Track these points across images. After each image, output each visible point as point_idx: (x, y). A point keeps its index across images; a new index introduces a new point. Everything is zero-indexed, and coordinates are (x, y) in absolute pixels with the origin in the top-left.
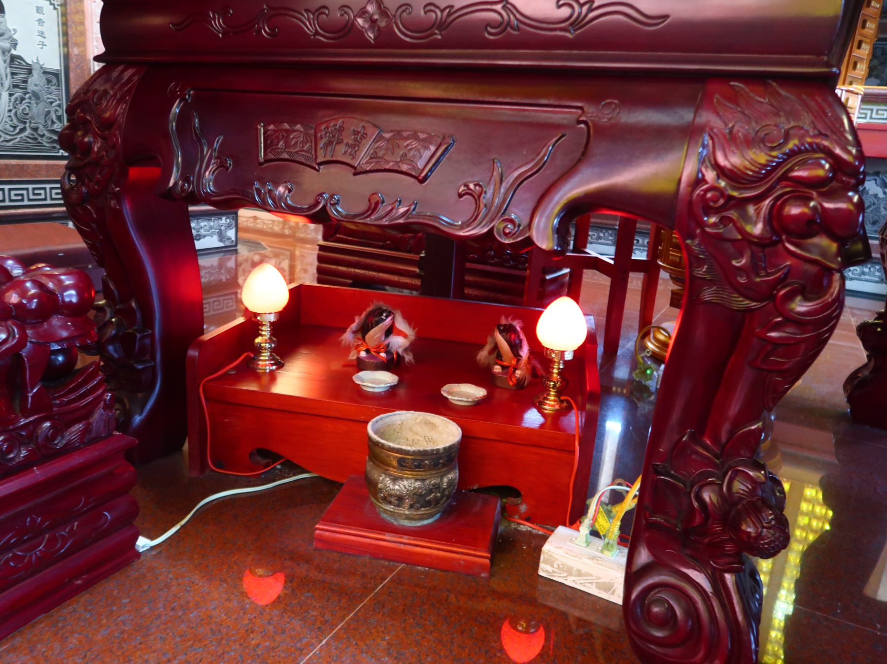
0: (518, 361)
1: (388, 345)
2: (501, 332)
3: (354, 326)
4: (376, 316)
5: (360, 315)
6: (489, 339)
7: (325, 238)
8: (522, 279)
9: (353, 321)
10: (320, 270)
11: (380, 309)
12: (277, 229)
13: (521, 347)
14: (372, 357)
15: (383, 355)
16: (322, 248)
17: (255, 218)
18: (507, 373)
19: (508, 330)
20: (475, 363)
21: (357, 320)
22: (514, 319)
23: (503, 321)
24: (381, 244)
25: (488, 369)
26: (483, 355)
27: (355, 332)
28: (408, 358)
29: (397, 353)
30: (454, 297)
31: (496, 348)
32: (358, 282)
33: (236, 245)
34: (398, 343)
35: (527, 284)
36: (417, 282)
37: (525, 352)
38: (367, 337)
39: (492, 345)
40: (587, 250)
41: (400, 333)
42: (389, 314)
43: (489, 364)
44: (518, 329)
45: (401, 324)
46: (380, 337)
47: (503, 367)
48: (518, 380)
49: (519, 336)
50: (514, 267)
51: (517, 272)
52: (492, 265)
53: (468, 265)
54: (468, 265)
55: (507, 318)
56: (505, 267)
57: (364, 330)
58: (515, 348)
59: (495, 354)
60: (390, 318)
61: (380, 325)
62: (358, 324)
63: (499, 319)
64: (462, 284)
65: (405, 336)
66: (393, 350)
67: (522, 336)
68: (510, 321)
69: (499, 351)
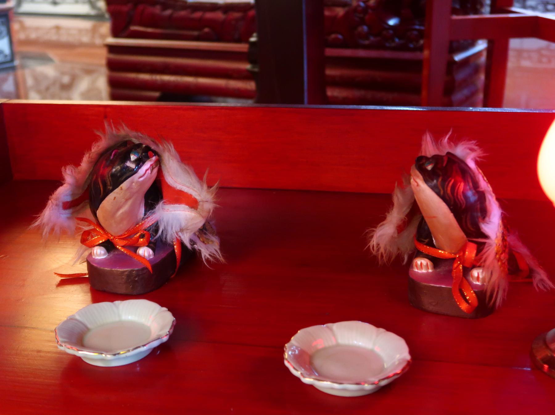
0: (480, 247)
1: (156, 227)
2: (428, 177)
3: (63, 193)
4: (112, 164)
5: (77, 163)
6: (398, 198)
7: (116, 32)
8: (417, 65)
9: (59, 182)
10: (113, 83)
11: (130, 142)
12: (85, 39)
13: (484, 213)
14: (121, 260)
15: (145, 252)
16: (112, 49)
17: (58, 28)
18: (447, 276)
19: (445, 172)
20: (367, 260)
21: (70, 176)
22: (455, 140)
23: (429, 148)
24: (196, 33)
25: (400, 266)
26: (384, 235)
27: (71, 205)
28: (209, 250)
29: (182, 244)
30: (310, 103)
31: (415, 210)
32: (169, 93)
33: (12, 60)
34: (179, 220)
35: (425, 72)
36: (251, 85)
37: (493, 226)
38: (99, 212)
39: (406, 210)
40: (514, 9)
41: (180, 197)
42: (146, 153)
43: (399, 257)
44: (472, 164)
45: (178, 177)
46: (131, 213)
47: (436, 261)
48: (481, 294)
49: (476, 186)
50: (403, 48)
51: (407, 55)
52: (365, 47)
53: (330, 52)
54: (330, 52)
55: (437, 139)
56: (386, 48)
57: (90, 196)
58: (469, 216)
59: (412, 231)
60: (147, 165)
61: (124, 185)
62: (77, 185)
63: (419, 145)
64: (320, 85)
65: (193, 204)
66: (171, 235)
67: (484, 185)
68: (446, 147)
69: (423, 219)
